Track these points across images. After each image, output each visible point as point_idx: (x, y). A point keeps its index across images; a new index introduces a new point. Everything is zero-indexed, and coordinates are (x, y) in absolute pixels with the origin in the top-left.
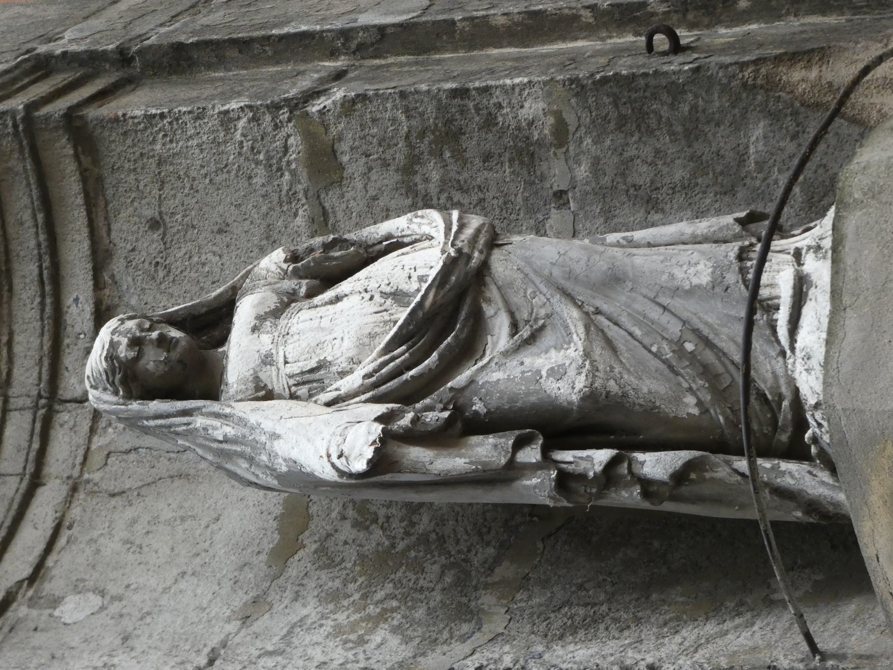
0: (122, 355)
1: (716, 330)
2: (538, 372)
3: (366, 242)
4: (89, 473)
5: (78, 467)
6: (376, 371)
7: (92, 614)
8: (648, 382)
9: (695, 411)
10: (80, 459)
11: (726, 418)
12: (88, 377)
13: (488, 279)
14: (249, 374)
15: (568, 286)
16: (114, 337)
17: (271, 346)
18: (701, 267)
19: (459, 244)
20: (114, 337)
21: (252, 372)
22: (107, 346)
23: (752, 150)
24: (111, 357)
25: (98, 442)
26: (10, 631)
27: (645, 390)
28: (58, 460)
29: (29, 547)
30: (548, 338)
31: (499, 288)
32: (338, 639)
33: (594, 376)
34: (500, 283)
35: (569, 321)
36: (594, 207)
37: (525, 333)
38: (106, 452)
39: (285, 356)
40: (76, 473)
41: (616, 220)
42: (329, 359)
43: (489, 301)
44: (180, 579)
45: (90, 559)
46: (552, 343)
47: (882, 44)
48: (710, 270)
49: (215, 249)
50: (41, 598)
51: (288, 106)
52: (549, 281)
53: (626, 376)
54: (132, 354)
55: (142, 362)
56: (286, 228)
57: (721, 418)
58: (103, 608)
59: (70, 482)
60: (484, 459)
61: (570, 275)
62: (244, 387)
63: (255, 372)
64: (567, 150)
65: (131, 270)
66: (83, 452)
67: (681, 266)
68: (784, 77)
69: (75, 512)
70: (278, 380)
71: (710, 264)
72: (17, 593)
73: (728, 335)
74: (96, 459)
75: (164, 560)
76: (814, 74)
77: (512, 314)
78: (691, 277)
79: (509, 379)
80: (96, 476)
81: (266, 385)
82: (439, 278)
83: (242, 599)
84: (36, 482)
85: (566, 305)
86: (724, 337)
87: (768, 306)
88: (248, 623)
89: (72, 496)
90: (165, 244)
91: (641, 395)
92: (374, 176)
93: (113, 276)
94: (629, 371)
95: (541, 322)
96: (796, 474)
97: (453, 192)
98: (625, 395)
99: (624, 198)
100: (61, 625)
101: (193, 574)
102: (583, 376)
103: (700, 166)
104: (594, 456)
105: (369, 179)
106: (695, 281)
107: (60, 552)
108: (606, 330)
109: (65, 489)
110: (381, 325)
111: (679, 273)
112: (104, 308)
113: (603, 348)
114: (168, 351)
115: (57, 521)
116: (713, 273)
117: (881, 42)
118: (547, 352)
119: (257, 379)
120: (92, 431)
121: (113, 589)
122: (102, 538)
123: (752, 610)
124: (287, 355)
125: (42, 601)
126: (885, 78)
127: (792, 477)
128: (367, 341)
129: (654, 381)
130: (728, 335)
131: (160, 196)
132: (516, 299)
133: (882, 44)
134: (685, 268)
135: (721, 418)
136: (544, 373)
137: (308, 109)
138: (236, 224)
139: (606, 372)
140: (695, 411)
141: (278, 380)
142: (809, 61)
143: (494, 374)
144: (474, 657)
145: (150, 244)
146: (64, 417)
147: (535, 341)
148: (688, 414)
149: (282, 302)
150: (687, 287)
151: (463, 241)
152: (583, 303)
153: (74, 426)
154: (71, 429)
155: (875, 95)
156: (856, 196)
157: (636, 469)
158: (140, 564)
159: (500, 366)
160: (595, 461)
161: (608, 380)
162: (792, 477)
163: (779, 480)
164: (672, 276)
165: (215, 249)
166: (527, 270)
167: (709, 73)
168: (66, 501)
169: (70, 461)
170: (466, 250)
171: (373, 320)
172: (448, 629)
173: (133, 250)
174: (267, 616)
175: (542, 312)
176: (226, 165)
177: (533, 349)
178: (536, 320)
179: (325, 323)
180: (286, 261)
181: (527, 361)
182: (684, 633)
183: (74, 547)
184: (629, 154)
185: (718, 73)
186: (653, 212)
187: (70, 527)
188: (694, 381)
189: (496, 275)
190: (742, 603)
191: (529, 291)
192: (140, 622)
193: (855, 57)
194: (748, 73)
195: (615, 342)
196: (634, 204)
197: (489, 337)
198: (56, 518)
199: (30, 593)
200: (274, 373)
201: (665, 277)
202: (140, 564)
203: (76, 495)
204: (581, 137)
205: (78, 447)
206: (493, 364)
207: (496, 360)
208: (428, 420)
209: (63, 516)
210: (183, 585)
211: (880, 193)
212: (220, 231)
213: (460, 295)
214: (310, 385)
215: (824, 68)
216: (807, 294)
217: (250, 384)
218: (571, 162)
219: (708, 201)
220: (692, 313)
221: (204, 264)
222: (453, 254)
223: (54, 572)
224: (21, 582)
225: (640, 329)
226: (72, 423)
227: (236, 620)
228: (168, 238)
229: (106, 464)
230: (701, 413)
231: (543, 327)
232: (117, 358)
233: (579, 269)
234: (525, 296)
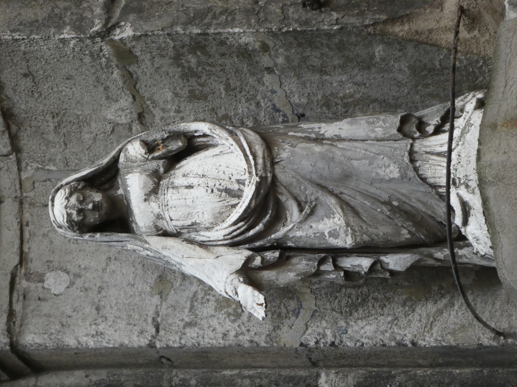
1: (409, 197)
2: (323, 234)
4: (26, 193)
5: (19, 191)
6: (230, 233)
7: (68, 287)
8: (381, 228)
9: (409, 236)
10: (18, 186)
11: (425, 236)
12: (54, 221)
13: (278, 184)
15: (322, 182)
16: (68, 210)
17: (159, 210)
18: (392, 168)
19: (260, 173)
21: (152, 223)
22: (65, 216)
23: (377, 54)
24: (70, 221)
26: (24, 297)
27: (382, 234)
28: (6, 188)
29: (10, 242)
30: (320, 211)
31: (285, 187)
32: (223, 312)
33: (355, 236)
34: (285, 184)
35: (331, 206)
36: (290, 73)
37: (307, 210)
38: (32, 182)
39: (170, 217)
40: (18, 194)
41: (303, 79)
42: (198, 221)
43: (282, 194)
44: (109, 263)
46: (323, 214)
47: (440, 10)
48: (398, 170)
49: (66, 85)
51: (100, 36)
53: (370, 230)
54: (80, 218)
56: (108, 78)
57: (423, 237)
58: (72, 284)
59: (18, 200)
60: (303, 271)
61: (321, 177)
63: (154, 223)
64: (270, 53)
65: (17, 93)
66: (18, 182)
67: (381, 168)
68: (390, 30)
69: (27, 216)
71: (396, 166)
72: (16, 272)
73: (415, 198)
74: (27, 185)
75: (94, 249)
76: (406, 27)
77: (296, 199)
78: (388, 174)
79: (307, 237)
81: (162, 228)
82: (255, 194)
85: (326, 196)
86: (414, 200)
87: (435, 186)
88: (164, 296)
89: (22, 207)
90: (35, 83)
91: (380, 237)
92: (156, 60)
93: (7, 96)
94: (370, 225)
95: (314, 203)
96: (468, 255)
97: (205, 67)
98: (372, 240)
99: (306, 70)
102: (350, 236)
104: (362, 264)
105: (154, 61)
106: (391, 176)
107: (28, 242)
108: (349, 202)
109: (17, 204)
110: (224, 208)
111: (381, 172)
112: (5, 110)
113: (353, 217)
114: (99, 211)
115: (20, 224)
116: (400, 171)
117: (438, 8)
118: (323, 220)
119: (156, 227)
120: (19, 170)
123: (449, 293)
124: (171, 216)
125: (33, 276)
126: (446, 27)
127: (467, 258)
128: (219, 215)
129: (384, 227)
130: (415, 198)
131: (27, 65)
132: (296, 191)
133: (440, 10)
134: (383, 169)
135: (423, 237)
136: (326, 234)
137: (112, 37)
138: (76, 76)
139: (360, 231)
140: (409, 236)
142: (402, 22)
143: (297, 233)
144: (310, 331)
147: (313, 213)
148: (405, 239)
149: (155, 183)
150: (388, 179)
151: (260, 171)
152: (333, 189)
153: (8, 169)
154: (7, 171)
155: (442, 34)
156: (490, 179)
157: (385, 266)
158: (80, 251)
159: (299, 228)
160: (363, 267)
161: (362, 235)
162: (467, 258)
163: (460, 260)
164: (377, 174)
165: (66, 85)
166: (297, 177)
167: (348, 30)
168: (20, 212)
169: (13, 188)
170: (264, 175)
171: (219, 205)
172: (282, 304)
173: (16, 85)
174: (172, 292)
175: (313, 198)
176: (66, 55)
177: (314, 218)
178: (311, 202)
179: (189, 202)
180: (146, 153)
181: (314, 225)
182: (418, 310)
183: (35, 239)
184: (306, 55)
185: (353, 30)
186: (324, 75)
187: (27, 225)
188: (404, 223)
189: (281, 180)
191: (302, 188)
192: (99, 296)
193: (427, 18)
195: (356, 208)
196: (313, 72)
197: (287, 212)
198: (18, 223)
199: (23, 271)
200: (165, 224)
201: (374, 174)
203: (23, 206)
204: (277, 49)
205: (15, 180)
206: (295, 228)
207: (296, 226)
208: (268, 258)
209: (21, 220)
210: (112, 267)
211: (503, 179)
212: (67, 79)
215: (411, 24)
216: (469, 212)
217: (153, 229)
218: (273, 57)
219: (356, 72)
220: (393, 190)
221: (61, 92)
222: (258, 180)
223: (31, 255)
224: (16, 267)
225: (369, 202)
226: (6, 168)
228: (36, 80)
229: (34, 188)
230: (412, 236)
231: (316, 206)
232: (73, 221)
233: (326, 173)
234: (301, 190)
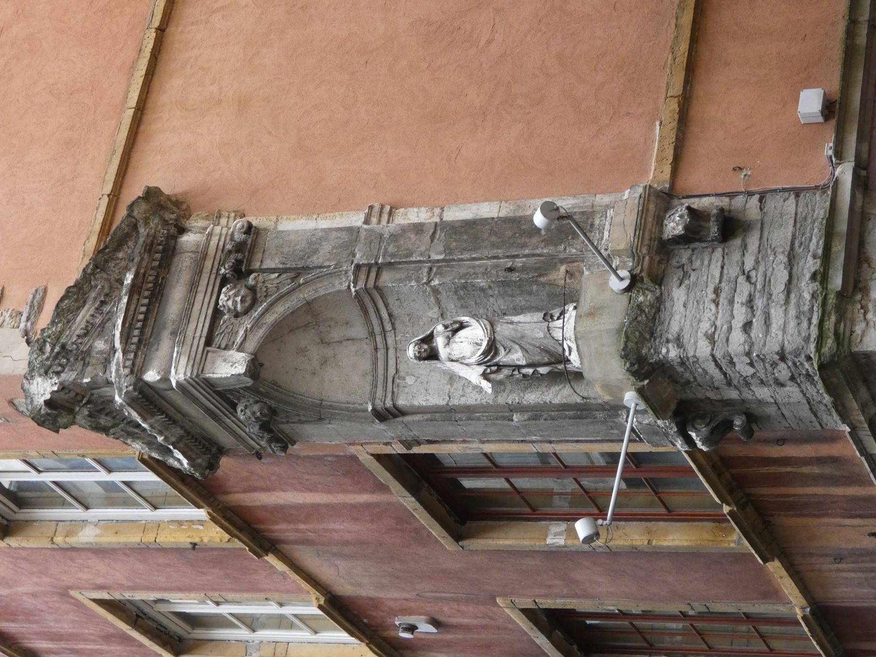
14: (447, 357)
25: (397, 339)
30: (513, 351)
37: (507, 350)
52: (509, 339)
54: (253, 283)
58: (416, 380)
61: (513, 337)
74: (398, 343)
76: (545, 279)
80: (400, 346)
84: (387, 349)
103: (522, 291)
109: (394, 350)
119: (449, 358)
120: (395, 336)
121: (417, 375)
145: (397, 303)
146: (388, 335)
159: (504, 358)
177: (510, 353)
190: (561, 380)
194: (531, 279)
213: (491, 346)
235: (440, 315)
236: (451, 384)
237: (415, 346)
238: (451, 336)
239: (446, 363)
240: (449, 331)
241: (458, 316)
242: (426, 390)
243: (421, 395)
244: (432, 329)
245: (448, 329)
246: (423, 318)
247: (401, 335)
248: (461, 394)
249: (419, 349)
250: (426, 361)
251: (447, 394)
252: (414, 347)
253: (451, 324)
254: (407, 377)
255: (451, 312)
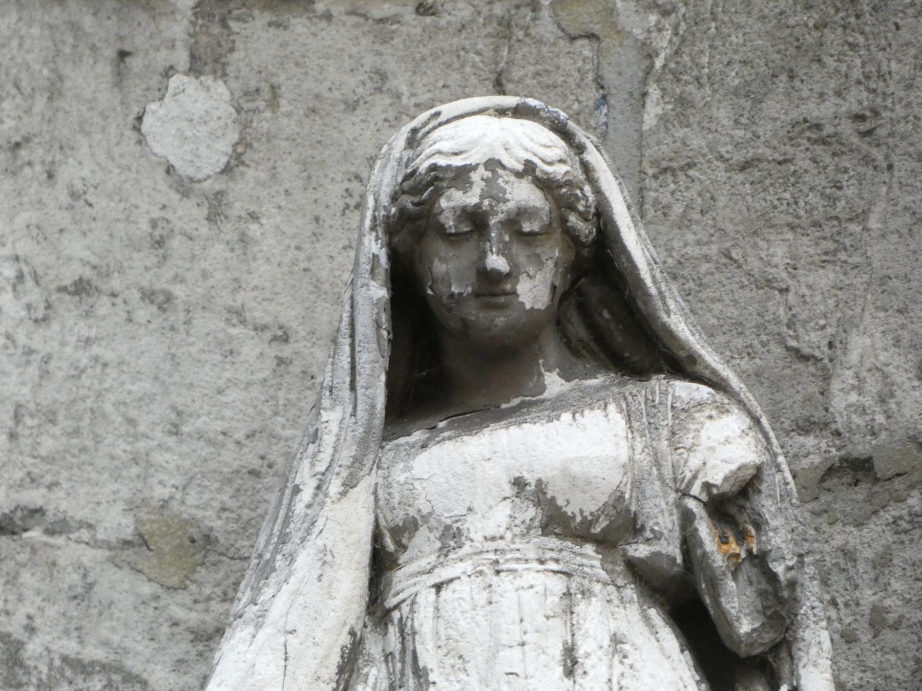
0: (443, 203)
3: (795, 639)
7: (170, 170)
12: (438, 114)
16: (481, 170)
20: (481, 170)
21: (426, 510)
22: (457, 162)
38: (597, 28)
45: (336, 94)
50: (224, 23)
54: (449, 222)
55: (440, 248)
62: (396, 501)
63: (426, 518)
70: (412, 576)
81: (405, 548)
83: (205, 507)
100: (135, 110)
101: (281, 361)
114: (476, 295)
119: (411, 526)
122: (388, 101)
125: (216, 29)
141: (412, 576)
149: (588, 524)
158: (317, 219)
180: (707, 486)
202: (317, 219)
214: (398, 656)
227: (138, 521)
232: (438, 193)
235: (861, 447)
236: (142, 541)
237: (546, 185)
238: (640, 551)
239: (362, 494)
240: (689, 542)
241: (848, 638)
242: (81, 288)
243: (38, 231)
244: (711, 358)
245: (705, 530)
246: (826, 278)
247: (663, 42)
248: (33, 648)
249: (513, 223)
250: (379, 292)
251: (34, 497)
252: (529, 169)
253: (760, 560)
254: (220, 89)
255: (883, 562)
